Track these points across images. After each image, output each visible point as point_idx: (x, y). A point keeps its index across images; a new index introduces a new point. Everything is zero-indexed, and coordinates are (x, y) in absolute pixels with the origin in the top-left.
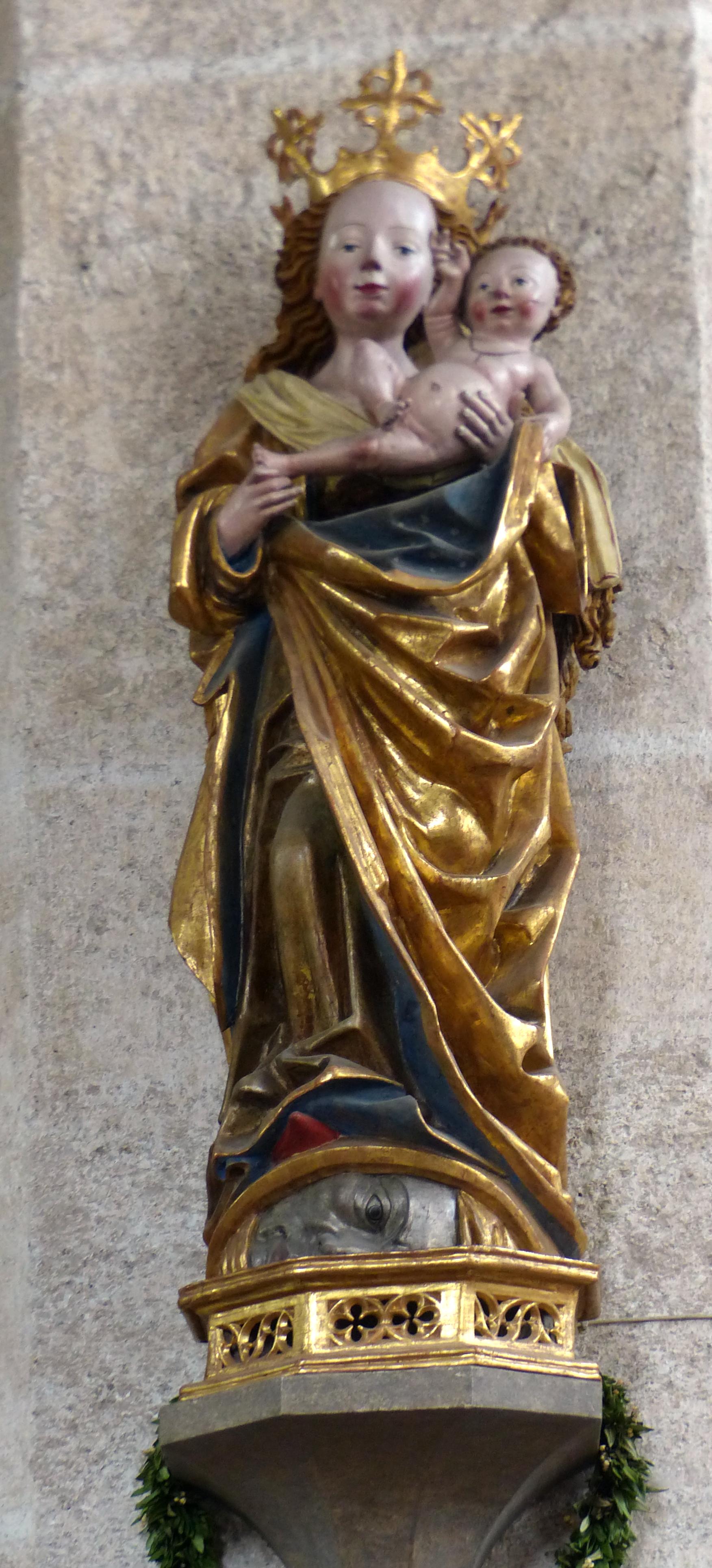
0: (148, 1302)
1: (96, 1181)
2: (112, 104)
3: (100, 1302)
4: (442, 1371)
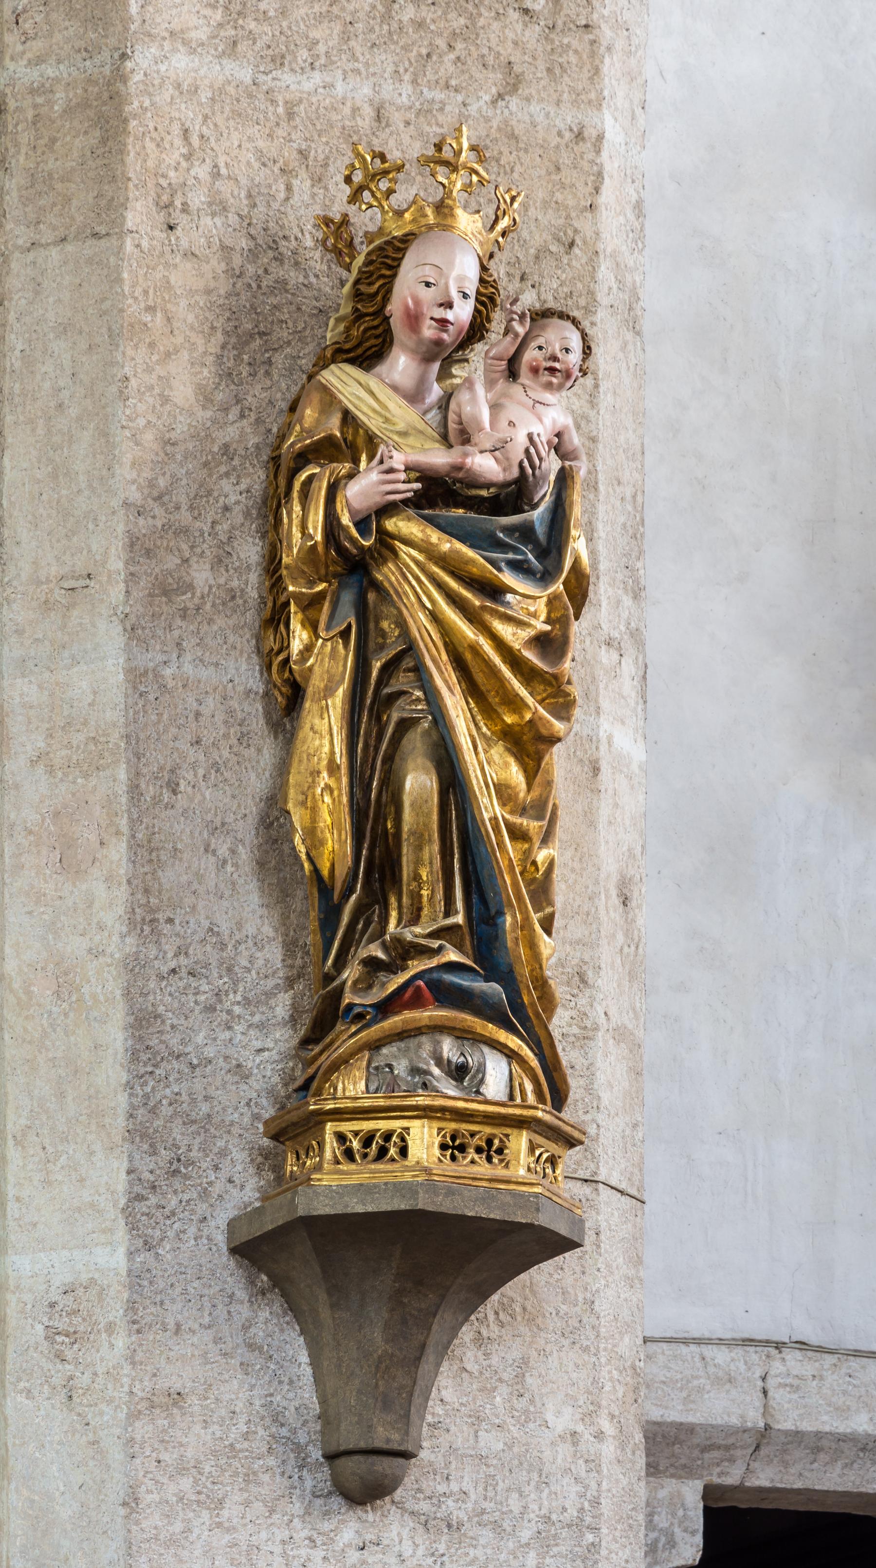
0: (207, 1098)
1: (170, 995)
2: (195, 90)
3: (172, 1092)
4: (521, 1195)
